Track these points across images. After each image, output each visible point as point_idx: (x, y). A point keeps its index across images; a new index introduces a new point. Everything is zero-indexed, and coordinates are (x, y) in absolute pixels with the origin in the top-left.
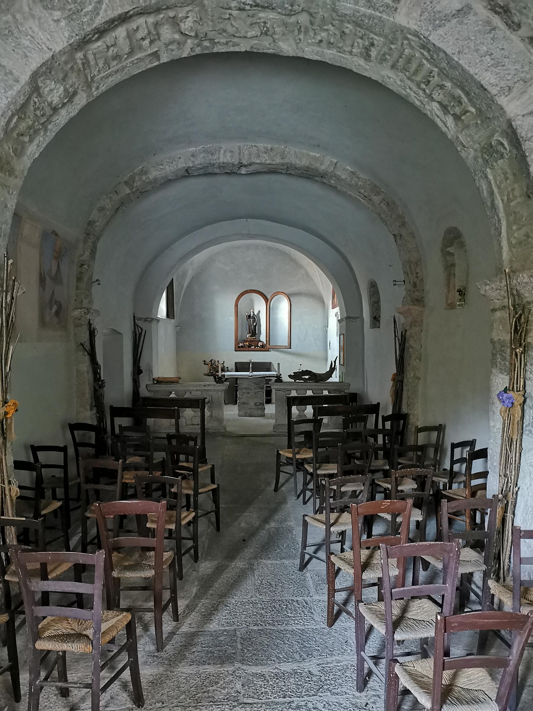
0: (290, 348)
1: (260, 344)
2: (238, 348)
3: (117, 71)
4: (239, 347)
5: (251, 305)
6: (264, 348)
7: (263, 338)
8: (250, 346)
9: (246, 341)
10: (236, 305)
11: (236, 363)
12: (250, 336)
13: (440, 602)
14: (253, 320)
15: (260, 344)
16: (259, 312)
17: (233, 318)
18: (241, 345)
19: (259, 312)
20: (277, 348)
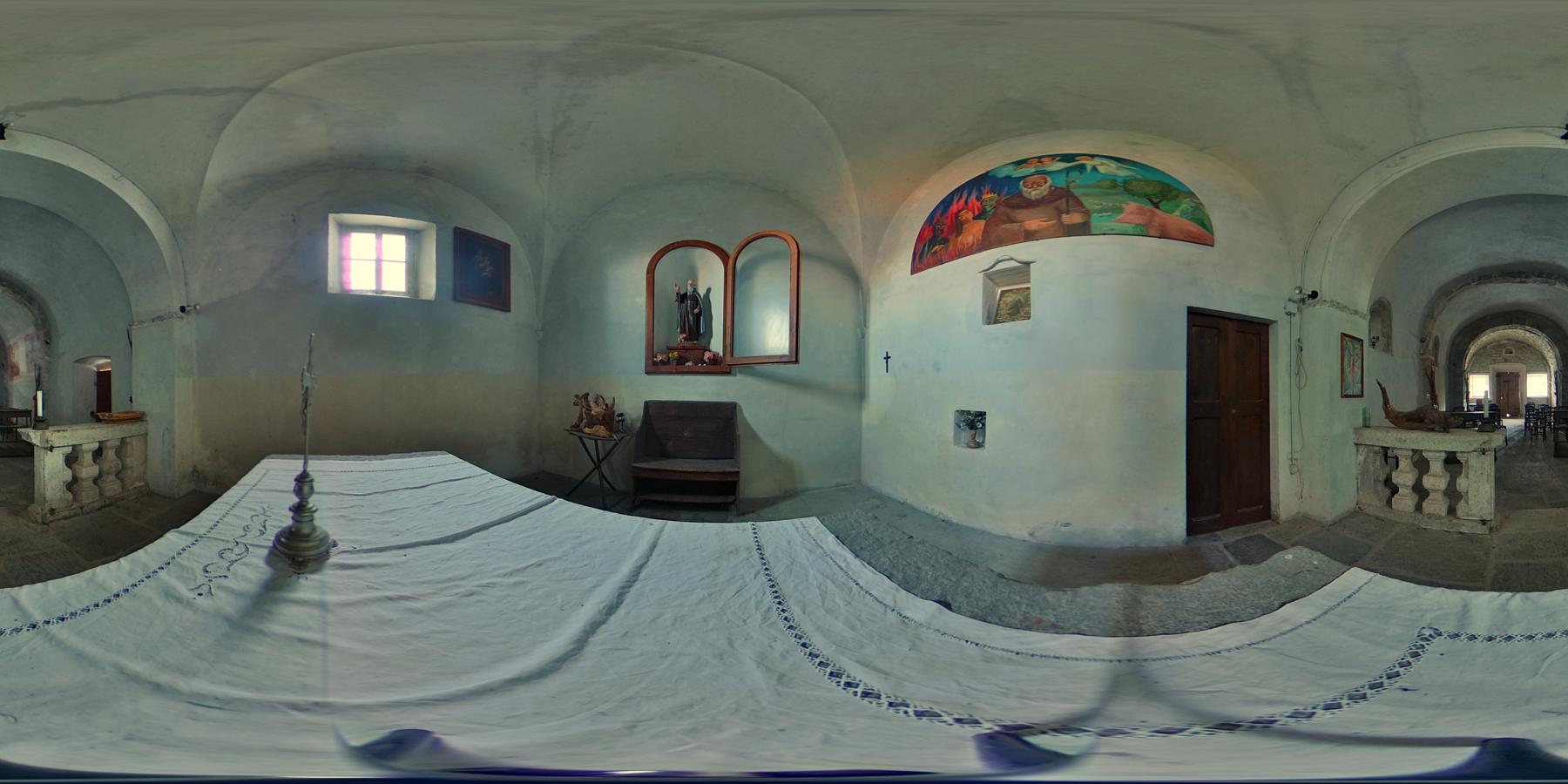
0: (797, 361)
1: (707, 355)
2: (655, 366)
3: (79, 656)
4: (655, 363)
5: (693, 274)
6: (718, 366)
7: (717, 345)
8: (681, 361)
9: (671, 349)
10: (651, 271)
11: (647, 404)
12: (686, 337)
13: (1194, 228)
14: (693, 309)
15: (707, 355)
16: (709, 290)
17: (641, 300)
18: (660, 358)
19: (709, 290)
20: (755, 366)
